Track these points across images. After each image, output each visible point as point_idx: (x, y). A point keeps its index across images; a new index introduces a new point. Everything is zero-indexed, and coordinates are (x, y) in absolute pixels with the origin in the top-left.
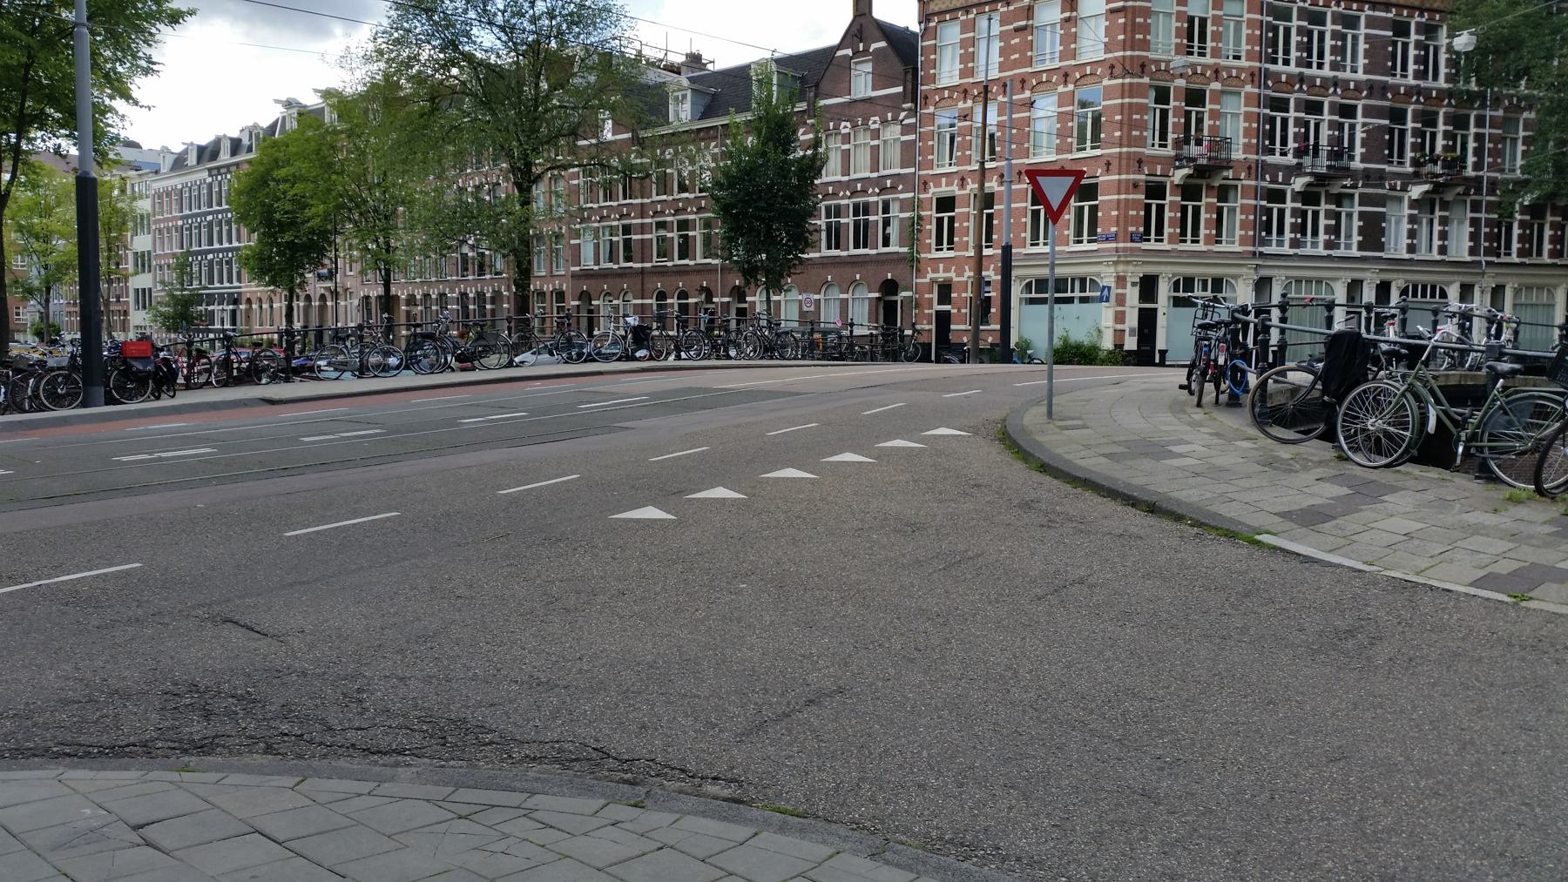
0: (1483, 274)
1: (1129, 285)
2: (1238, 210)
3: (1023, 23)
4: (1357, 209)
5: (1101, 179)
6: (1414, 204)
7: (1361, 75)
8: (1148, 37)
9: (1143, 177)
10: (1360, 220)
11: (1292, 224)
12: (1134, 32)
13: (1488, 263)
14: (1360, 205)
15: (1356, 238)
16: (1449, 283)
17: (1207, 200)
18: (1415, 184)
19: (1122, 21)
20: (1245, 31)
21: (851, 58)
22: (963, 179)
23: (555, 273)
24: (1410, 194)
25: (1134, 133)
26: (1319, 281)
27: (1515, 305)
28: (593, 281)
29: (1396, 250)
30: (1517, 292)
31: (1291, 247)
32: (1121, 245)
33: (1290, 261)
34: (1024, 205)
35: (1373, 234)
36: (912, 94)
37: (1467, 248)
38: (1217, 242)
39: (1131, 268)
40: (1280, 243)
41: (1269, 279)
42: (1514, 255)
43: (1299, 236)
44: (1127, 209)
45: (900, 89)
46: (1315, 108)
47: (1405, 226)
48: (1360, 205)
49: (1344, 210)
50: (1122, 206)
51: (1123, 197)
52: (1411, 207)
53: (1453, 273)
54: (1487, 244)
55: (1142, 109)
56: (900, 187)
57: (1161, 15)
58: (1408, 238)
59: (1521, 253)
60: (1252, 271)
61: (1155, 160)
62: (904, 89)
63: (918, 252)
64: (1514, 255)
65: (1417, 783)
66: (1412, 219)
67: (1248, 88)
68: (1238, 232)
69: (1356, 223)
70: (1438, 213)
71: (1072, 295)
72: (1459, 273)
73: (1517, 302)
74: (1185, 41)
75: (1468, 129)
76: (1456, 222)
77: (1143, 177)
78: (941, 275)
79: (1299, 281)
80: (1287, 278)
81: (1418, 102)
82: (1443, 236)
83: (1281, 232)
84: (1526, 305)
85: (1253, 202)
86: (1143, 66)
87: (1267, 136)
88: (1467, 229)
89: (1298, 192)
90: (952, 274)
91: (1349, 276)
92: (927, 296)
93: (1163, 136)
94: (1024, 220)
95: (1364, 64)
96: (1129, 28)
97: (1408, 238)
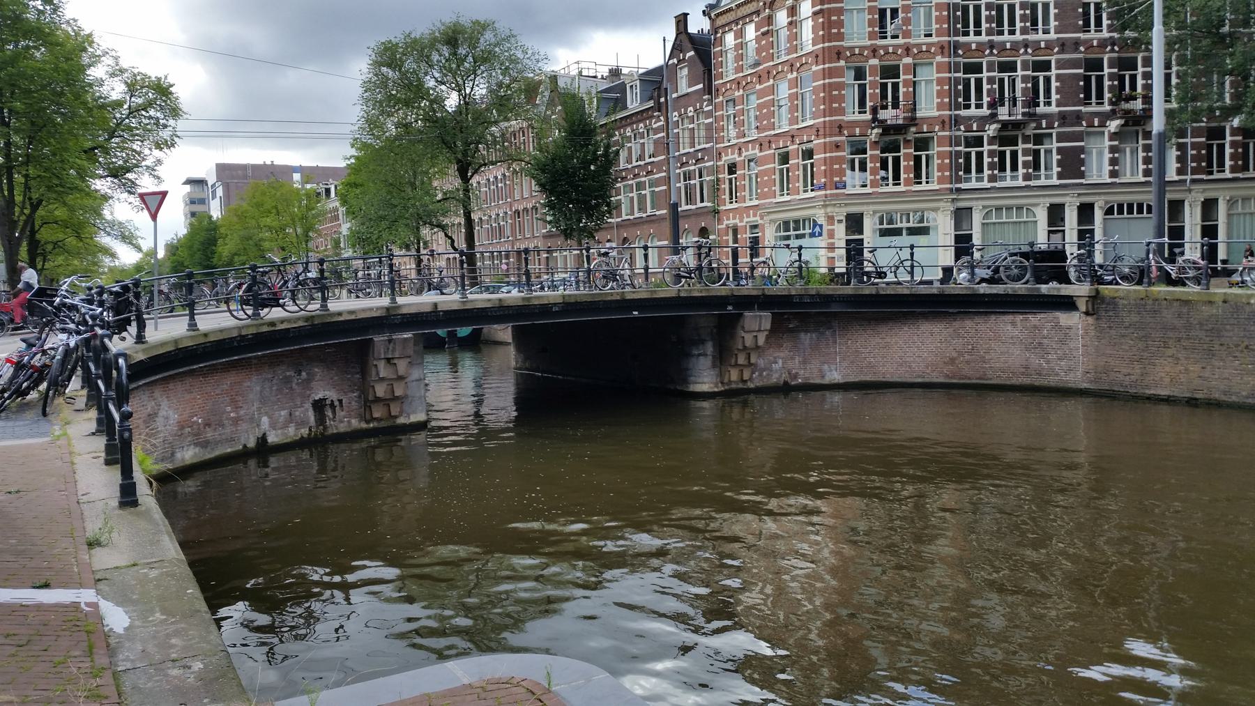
3: (766, 29)
4: (1055, 145)
6: (1113, 136)
7: (1053, 36)
8: (842, 30)
10: (1058, 154)
12: (830, 28)
13: (1193, 181)
15: (1056, 169)
17: (906, 152)
18: (1112, 120)
19: (821, 20)
20: (934, 14)
21: (677, 65)
22: (740, 149)
25: (834, 105)
26: (1019, 208)
27: (1229, 216)
29: (1101, 176)
30: (1232, 203)
31: (989, 181)
32: (828, 192)
34: (772, 165)
35: (1072, 164)
36: (709, 89)
37: (1175, 170)
39: (837, 210)
42: (1227, 171)
43: (996, 172)
44: (832, 165)
45: (701, 86)
46: (1011, 67)
49: (1042, 148)
52: (1111, 140)
54: (1194, 164)
55: (841, 86)
56: (706, 158)
57: (855, 12)
59: (1233, 170)
60: (949, 204)
61: (854, 124)
62: (704, 85)
63: (718, 206)
64: (1227, 171)
66: (1113, 150)
67: (939, 58)
68: (937, 174)
69: (1056, 157)
70: (1141, 142)
71: (804, 232)
73: (1232, 212)
74: (877, 29)
75: (1136, 69)
78: (731, 222)
81: (1112, 51)
83: (980, 170)
86: (839, 54)
87: (960, 94)
89: (1114, 133)
90: (737, 221)
91: (1048, 201)
92: (724, 238)
93: (862, 103)
95: (1055, 26)
96: (826, 25)
97: (1110, 165)
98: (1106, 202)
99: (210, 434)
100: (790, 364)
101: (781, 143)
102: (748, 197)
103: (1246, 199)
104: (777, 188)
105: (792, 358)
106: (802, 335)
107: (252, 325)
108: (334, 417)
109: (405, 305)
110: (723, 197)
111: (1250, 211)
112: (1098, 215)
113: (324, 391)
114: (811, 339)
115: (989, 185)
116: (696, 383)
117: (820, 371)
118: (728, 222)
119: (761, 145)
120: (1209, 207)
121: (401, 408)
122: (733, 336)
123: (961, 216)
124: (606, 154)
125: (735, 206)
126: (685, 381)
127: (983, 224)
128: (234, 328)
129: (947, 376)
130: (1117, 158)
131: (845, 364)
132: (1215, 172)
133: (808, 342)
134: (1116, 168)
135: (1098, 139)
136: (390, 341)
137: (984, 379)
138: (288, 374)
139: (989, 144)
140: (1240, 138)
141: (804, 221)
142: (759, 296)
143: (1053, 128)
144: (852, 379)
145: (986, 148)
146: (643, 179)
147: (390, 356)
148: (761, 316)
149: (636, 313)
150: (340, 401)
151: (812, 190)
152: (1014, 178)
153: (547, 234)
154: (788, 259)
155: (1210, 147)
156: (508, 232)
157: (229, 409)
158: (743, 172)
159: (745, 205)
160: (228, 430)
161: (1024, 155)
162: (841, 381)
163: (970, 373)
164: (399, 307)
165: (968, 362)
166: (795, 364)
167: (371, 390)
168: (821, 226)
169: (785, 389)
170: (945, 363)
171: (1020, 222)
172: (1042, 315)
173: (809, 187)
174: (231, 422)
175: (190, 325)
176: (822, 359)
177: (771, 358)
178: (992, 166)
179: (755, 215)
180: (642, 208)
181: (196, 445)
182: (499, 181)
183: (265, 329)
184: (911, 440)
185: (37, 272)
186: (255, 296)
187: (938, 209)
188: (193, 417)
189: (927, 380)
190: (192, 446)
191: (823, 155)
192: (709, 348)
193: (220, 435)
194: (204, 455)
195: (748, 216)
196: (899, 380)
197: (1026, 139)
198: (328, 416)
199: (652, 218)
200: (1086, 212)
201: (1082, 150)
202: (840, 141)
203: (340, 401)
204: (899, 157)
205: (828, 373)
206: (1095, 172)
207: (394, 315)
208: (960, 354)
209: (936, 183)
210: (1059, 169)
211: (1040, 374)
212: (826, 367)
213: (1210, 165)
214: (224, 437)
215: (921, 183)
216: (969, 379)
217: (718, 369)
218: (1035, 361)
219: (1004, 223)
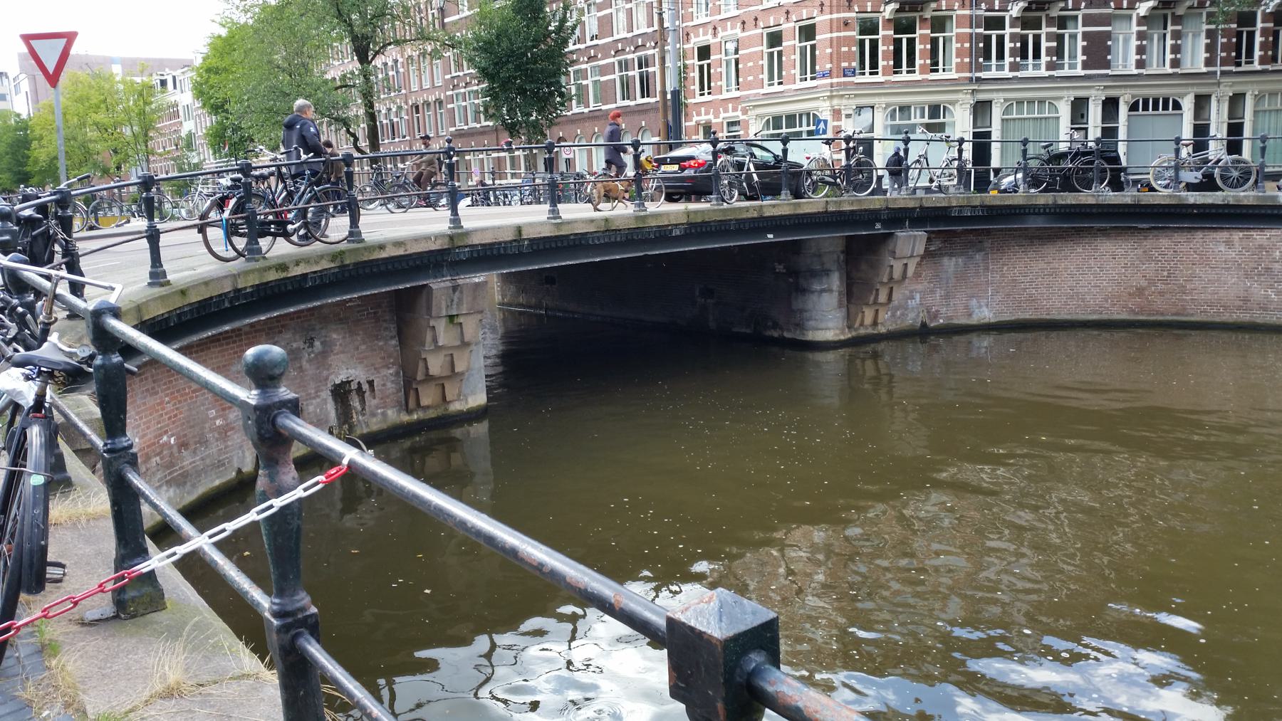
0: (1219, 84)
1: (843, 116)
2: (954, 39)
4: (1081, 29)
5: (817, 19)
6: (1143, 20)
9: (854, 15)
10: (1084, 40)
11: (1011, 49)
13: (1223, 73)
14: (1083, 26)
15: (1081, 58)
16: (1183, 96)
17: (922, 32)
22: (715, 29)
23: (441, 134)
24: (1138, 11)
26: (1041, 102)
27: (1256, 113)
28: (464, 139)
29: (1125, 67)
30: (1258, 99)
31: (1010, 71)
32: (835, 80)
33: (1137, 80)
34: (760, 48)
35: (1098, 52)
37: (1203, 59)
38: (932, 71)
39: (844, 102)
40: (1072, 66)
41: (989, 103)
42: (1256, 63)
43: (1018, 59)
44: (839, 47)
47: (1134, 43)
48: (1083, 26)
49: (1067, 32)
50: (835, 43)
51: (835, 35)
52: (1139, 24)
53: (1246, 82)
54: (1224, 54)
58: (1137, 54)
60: (969, 96)
63: (686, 98)
64: (1256, 63)
65: (1069, 589)
66: (1141, 36)
68: (955, 60)
69: (1081, 43)
70: (1170, 28)
72: (1193, 85)
73: (1257, 109)
76: (1190, 35)
77: (854, 15)
78: (703, 118)
79: (1020, 102)
80: (1006, 100)
82: (1176, 49)
83: (1000, 56)
84: (1270, 111)
85: (968, 30)
88: (1203, 41)
90: (711, 117)
94: (761, 62)
97: (1137, 54)
98: (1133, 97)
99: (188, 461)
100: (929, 300)
101: (772, 18)
102: (724, 88)
103: (1273, 94)
104: (765, 76)
105: (932, 292)
106: (946, 260)
107: (252, 271)
108: (363, 409)
109: (476, 231)
110: (692, 87)
111: (1276, 108)
112: (1123, 110)
113: (347, 370)
114: (957, 264)
115: (1011, 75)
116: (818, 329)
117: (967, 307)
118: (699, 118)
119: (744, 23)
120: (1236, 101)
121: (460, 388)
122: (875, 266)
123: (981, 109)
124: (560, 29)
125: (707, 98)
126: (800, 326)
127: (1003, 120)
128: (226, 277)
129: (1132, 311)
130: (1145, 46)
131: (999, 297)
132: (1243, 64)
133: (951, 269)
134: (1144, 57)
135: (1124, 24)
136: (455, 288)
137: (1183, 315)
138: (295, 345)
139: (1011, 27)
140: (1271, 25)
141: (801, 116)
142: (915, 208)
143: (1079, 9)
144: (1007, 317)
145: (1008, 31)
146: (584, 66)
147: (455, 313)
148: (915, 236)
149: (770, 236)
150: (371, 383)
151: (812, 79)
152: (1000, 68)
153: (456, 133)
154: (945, 156)
155: (1239, 35)
156: (404, 130)
157: (213, 413)
158: (718, 56)
159: (721, 97)
160: (213, 450)
161: (1048, 40)
162: (993, 321)
163: (1164, 309)
164: (467, 234)
165: (1161, 293)
166: (936, 300)
167: (421, 365)
168: (826, 122)
169: (923, 333)
170: (1130, 294)
171: (1041, 119)
172: (1274, 232)
173: (809, 75)
174: (216, 435)
175: (152, 275)
176: (969, 291)
177: (907, 292)
178: (1013, 53)
179: (735, 109)
180: (627, 94)
181: (169, 483)
182: (390, 68)
183: (272, 276)
184: (1059, 387)
185: (926, 250)
186: (250, 220)
187: (957, 101)
188: (161, 436)
189: (1105, 317)
190: (165, 488)
191: (829, 35)
192: (835, 281)
193: (203, 459)
194: (182, 498)
195: (726, 111)
196: (1069, 317)
197: (1051, 22)
198: (355, 408)
199: (597, 114)
200: (1110, 106)
201: (1108, 35)
202: (850, 18)
203: (371, 383)
204: (915, 38)
205: (977, 310)
206: (1120, 62)
207: (459, 247)
208: (1152, 282)
209: (954, 70)
210: (1085, 58)
211: (1265, 309)
212: (974, 302)
213: (1239, 56)
214: (208, 461)
215: (937, 71)
216: (1162, 314)
217: (844, 310)
218: (1259, 291)
219: (1024, 119)
